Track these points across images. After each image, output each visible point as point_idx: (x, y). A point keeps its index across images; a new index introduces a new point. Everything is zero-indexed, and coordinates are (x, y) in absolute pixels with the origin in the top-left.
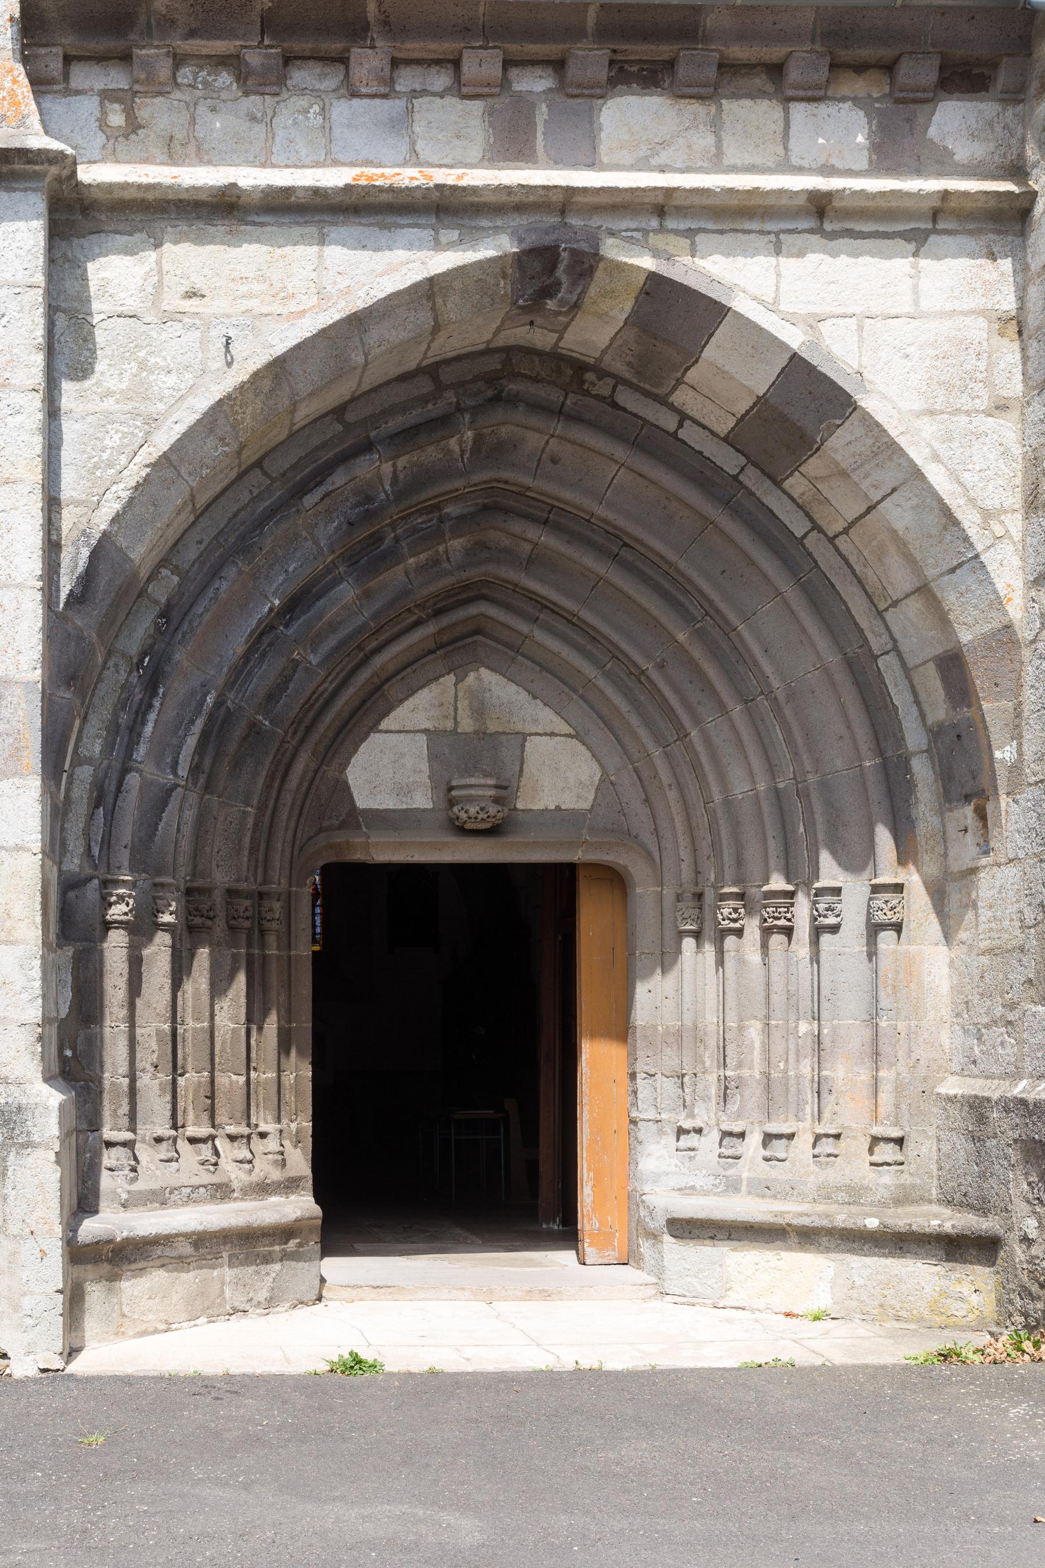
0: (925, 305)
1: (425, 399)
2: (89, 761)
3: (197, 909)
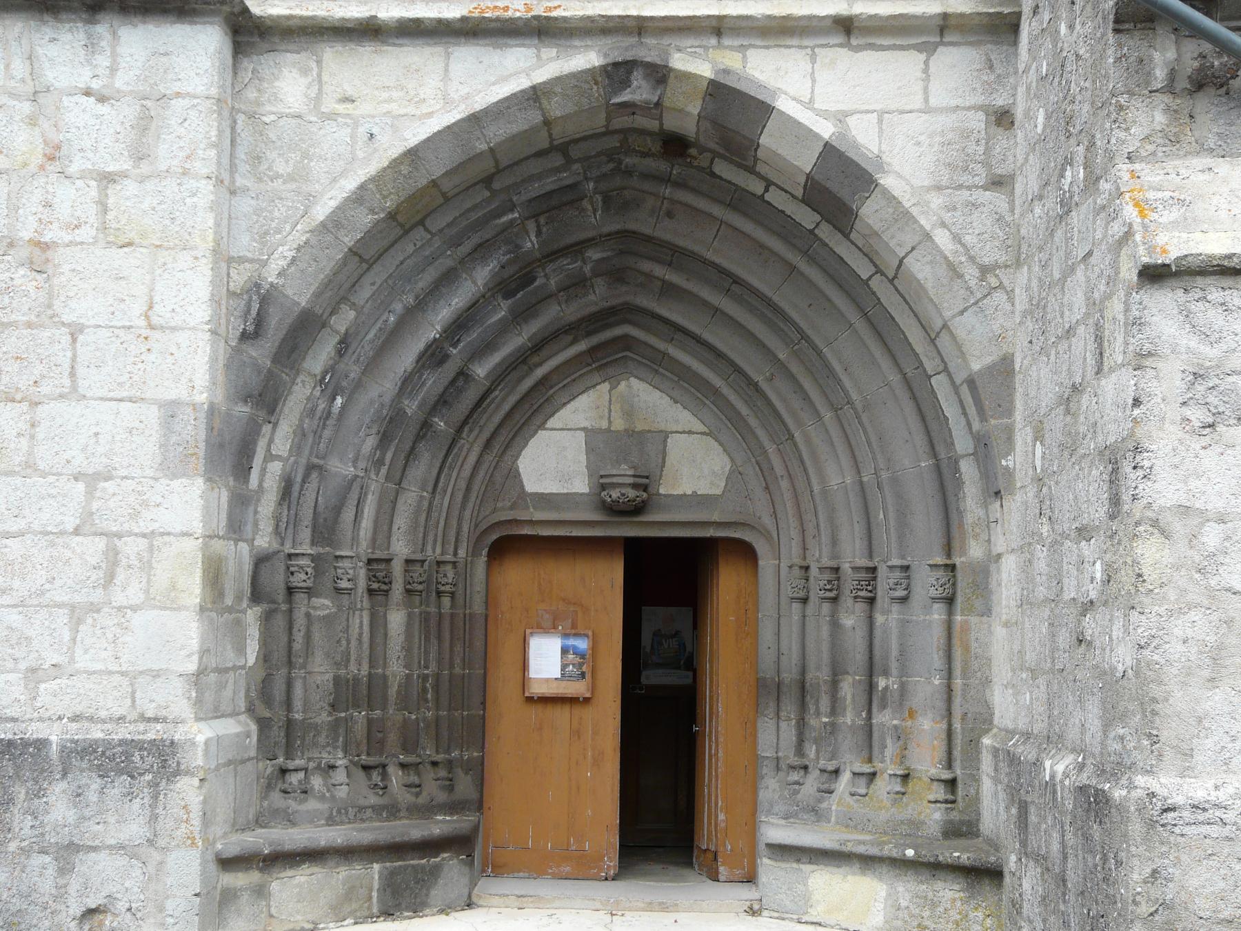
0: (933, 102)
1: (557, 170)
2: (278, 458)
3: (374, 576)
